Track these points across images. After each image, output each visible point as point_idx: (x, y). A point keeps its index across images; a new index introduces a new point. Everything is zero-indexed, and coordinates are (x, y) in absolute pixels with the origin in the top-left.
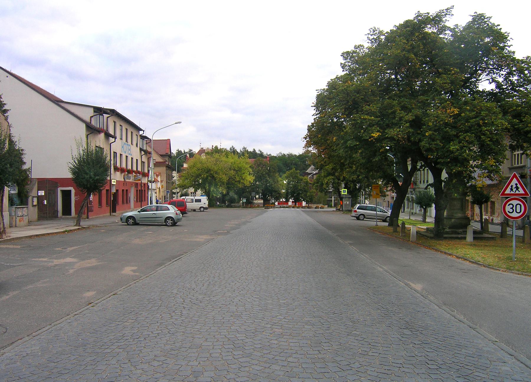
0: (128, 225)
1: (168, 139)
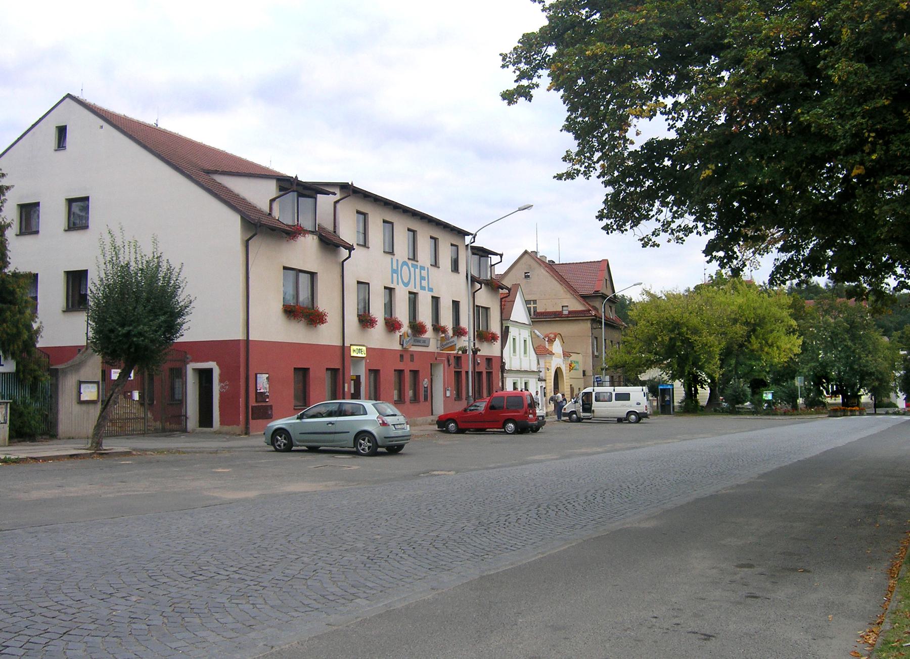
0: (277, 450)
1: (603, 260)
